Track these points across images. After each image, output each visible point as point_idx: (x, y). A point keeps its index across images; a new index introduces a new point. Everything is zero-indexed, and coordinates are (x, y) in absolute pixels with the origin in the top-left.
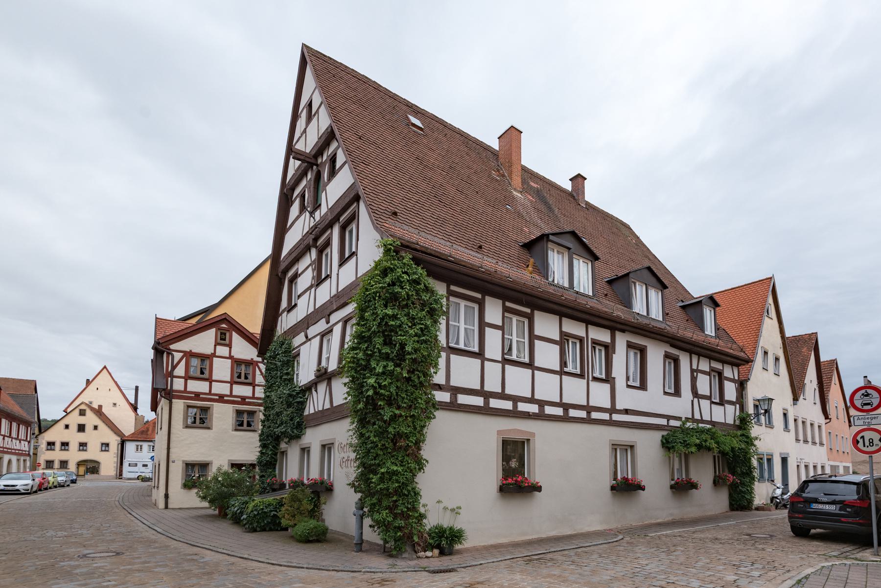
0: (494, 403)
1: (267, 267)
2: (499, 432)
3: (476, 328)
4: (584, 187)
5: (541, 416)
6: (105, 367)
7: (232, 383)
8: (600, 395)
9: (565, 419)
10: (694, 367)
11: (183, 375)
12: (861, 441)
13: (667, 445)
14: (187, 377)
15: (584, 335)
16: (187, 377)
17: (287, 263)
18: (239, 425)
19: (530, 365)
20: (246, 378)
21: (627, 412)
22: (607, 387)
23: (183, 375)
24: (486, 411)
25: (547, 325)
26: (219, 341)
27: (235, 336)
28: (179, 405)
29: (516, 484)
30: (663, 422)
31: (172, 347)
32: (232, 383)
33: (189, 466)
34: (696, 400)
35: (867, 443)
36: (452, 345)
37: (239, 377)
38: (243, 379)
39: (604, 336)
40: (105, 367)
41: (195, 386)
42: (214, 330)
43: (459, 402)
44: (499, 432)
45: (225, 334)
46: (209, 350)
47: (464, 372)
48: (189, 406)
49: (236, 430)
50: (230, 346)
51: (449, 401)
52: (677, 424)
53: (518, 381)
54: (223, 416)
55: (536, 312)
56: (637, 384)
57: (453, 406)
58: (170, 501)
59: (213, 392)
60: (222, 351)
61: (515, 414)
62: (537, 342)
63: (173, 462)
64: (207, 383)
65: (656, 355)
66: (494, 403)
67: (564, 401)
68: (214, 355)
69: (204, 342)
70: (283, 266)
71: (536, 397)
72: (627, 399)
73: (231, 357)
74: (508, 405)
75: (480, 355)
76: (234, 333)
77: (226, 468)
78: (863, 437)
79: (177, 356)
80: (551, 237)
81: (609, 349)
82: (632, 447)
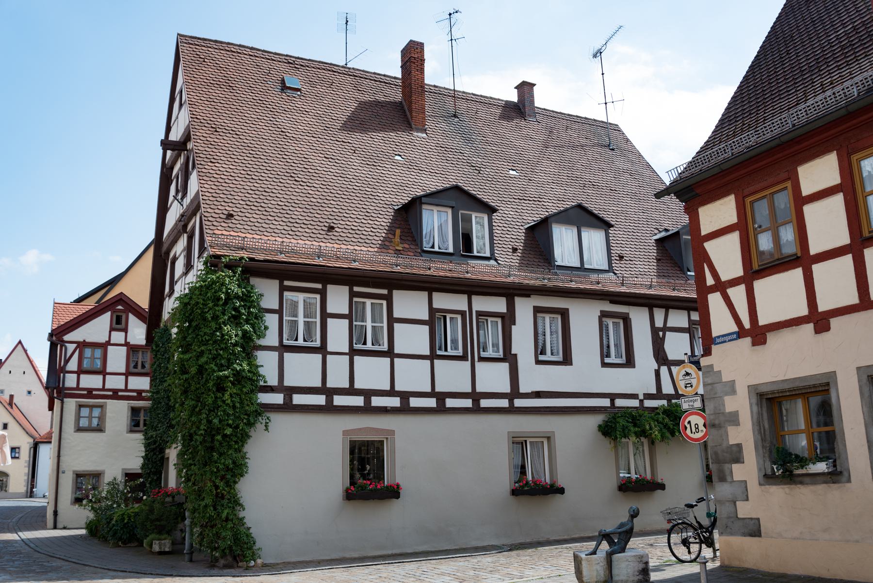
0: (339, 401)
1: (152, 249)
2: (345, 433)
4: (533, 96)
5: (405, 409)
6: (20, 342)
7: (128, 374)
8: (493, 378)
9: (441, 409)
10: (659, 323)
11: (76, 369)
12: (688, 426)
13: (607, 430)
14: (80, 371)
15: (465, 307)
16: (80, 371)
17: (169, 242)
18: (135, 426)
19: (390, 353)
20: (143, 367)
21: (538, 395)
22: (505, 367)
23: (76, 369)
24: (329, 409)
25: (410, 304)
26: (114, 325)
27: (131, 317)
28: (71, 404)
30: (606, 402)
31: (66, 338)
32: (128, 374)
33: (78, 475)
34: (664, 370)
35: (694, 430)
36: (285, 342)
37: (136, 367)
38: (139, 369)
39: (498, 305)
40: (20, 342)
41: (91, 381)
44: (345, 433)
46: (103, 339)
47: (302, 370)
48: (81, 406)
50: (125, 330)
52: (635, 403)
53: (372, 373)
54: (118, 413)
55: (395, 292)
56: (560, 358)
57: (288, 407)
58: (59, 518)
59: (107, 387)
61: (368, 409)
62: (396, 325)
63: (63, 472)
64: (101, 377)
65: (584, 320)
66: (339, 401)
67: (438, 389)
69: (97, 330)
71: (397, 388)
72: (533, 378)
73: (126, 344)
74: (359, 401)
75: (322, 350)
76: (130, 315)
77: (120, 478)
78: (689, 422)
79: (71, 347)
80: (424, 200)
81: (508, 319)
82: (548, 438)
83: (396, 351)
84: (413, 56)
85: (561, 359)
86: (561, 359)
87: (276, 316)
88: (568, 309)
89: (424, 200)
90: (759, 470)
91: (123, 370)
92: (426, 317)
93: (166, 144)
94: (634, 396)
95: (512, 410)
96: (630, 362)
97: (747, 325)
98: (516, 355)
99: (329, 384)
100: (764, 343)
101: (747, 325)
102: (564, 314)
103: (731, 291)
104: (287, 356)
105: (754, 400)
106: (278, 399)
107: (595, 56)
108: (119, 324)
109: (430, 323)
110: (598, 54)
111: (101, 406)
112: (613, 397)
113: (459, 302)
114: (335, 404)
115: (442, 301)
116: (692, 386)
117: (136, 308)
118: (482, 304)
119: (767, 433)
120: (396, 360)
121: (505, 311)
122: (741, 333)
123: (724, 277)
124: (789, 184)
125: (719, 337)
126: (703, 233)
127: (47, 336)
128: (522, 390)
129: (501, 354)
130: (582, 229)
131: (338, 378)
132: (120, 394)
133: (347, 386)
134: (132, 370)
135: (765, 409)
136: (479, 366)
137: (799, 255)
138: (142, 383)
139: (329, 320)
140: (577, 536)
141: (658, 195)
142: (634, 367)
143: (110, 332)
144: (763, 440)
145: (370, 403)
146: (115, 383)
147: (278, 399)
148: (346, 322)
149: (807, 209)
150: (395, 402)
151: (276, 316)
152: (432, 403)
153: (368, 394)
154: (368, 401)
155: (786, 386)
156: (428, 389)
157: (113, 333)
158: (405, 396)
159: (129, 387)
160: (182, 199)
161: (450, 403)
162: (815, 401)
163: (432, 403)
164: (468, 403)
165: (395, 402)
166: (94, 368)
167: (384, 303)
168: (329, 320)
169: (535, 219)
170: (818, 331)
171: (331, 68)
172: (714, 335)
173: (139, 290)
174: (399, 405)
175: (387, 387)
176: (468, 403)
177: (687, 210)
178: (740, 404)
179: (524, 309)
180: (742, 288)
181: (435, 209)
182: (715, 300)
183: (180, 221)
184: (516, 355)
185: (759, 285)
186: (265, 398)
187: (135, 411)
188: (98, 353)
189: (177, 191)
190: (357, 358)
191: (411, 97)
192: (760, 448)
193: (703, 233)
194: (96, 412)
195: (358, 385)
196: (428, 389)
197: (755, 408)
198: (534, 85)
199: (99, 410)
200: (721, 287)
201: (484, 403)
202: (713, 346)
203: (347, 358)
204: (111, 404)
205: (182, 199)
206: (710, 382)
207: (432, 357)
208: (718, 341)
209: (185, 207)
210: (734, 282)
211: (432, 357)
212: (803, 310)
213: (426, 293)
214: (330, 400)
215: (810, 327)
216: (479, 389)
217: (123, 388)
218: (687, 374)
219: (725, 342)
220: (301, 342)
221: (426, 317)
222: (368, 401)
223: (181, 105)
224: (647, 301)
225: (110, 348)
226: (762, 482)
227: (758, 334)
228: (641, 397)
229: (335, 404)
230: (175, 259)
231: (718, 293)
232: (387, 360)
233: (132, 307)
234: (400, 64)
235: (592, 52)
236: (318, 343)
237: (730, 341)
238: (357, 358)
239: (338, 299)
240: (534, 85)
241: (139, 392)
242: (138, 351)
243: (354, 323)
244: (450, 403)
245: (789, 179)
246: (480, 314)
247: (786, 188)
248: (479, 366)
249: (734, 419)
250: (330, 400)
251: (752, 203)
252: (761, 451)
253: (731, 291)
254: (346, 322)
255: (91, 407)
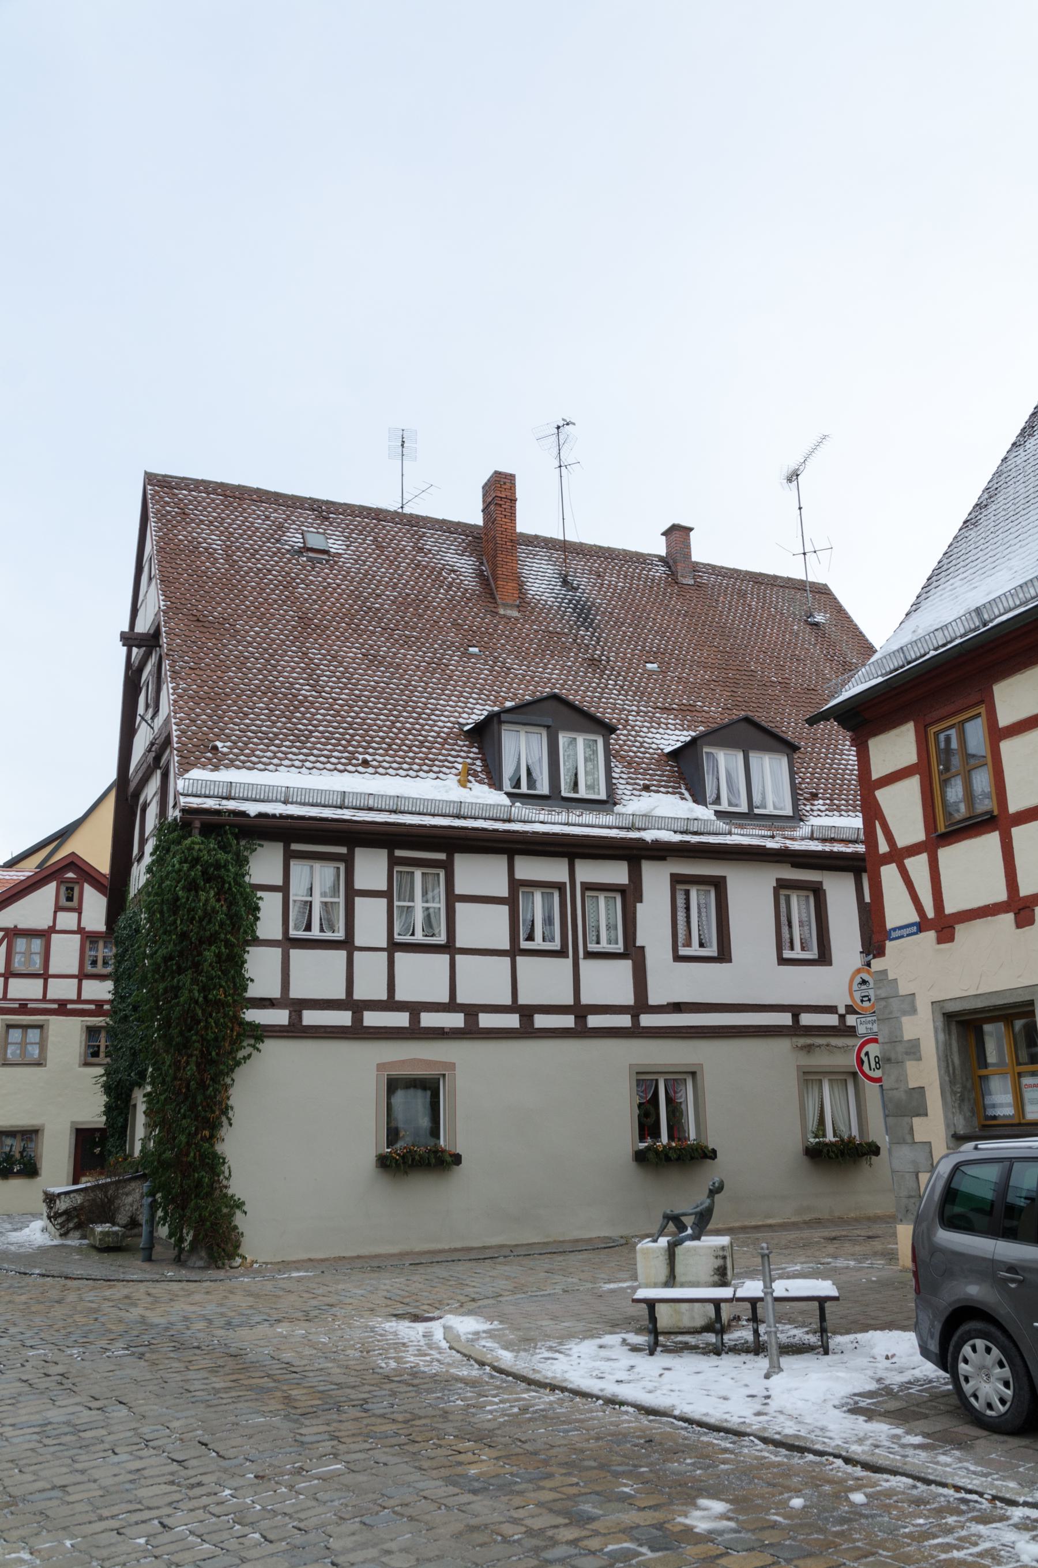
2: (380, 1067)
3: (341, 900)
5: (471, 1032)
7: (82, 976)
9: (527, 1031)
19: (449, 948)
21: (677, 1008)
24: (357, 1032)
26: (63, 902)
29: (415, 1155)
32: (82, 976)
36: (293, 933)
38: (100, 969)
39: (617, 873)
42: (54, 884)
43: (305, 1022)
44: (380, 1067)
45: (72, 889)
46: (44, 923)
47: (317, 975)
48: (9, 1026)
49: (86, 1064)
50: (79, 910)
51: (286, 1023)
53: (422, 978)
54: (67, 1035)
57: (295, 1031)
59: (49, 997)
60: (67, 920)
61: (415, 1033)
65: (751, 895)
66: (372, 1019)
67: (522, 1000)
68: (52, 930)
70: (133, 785)
71: (460, 999)
72: (668, 981)
73: (80, 930)
75: (347, 944)
76: (86, 886)
78: (867, 1054)
80: (503, 717)
81: (630, 895)
82: (693, 1074)
83: (458, 945)
84: (500, 492)
85: (715, 954)
86: (715, 954)
87: (279, 896)
88: (724, 878)
89: (503, 717)
90: (947, 1126)
91: (75, 971)
92: (504, 893)
93: (129, 639)
94: (831, 1009)
95: (636, 1032)
96: (824, 958)
97: (930, 914)
98: (643, 948)
99: (357, 996)
100: (951, 939)
101: (930, 914)
102: (719, 885)
103: (909, 862)
104: (294, 953)
105: (940, 1024)
106: (280, 1017)
107: (790, 480)
108: (69, 901)
109: (511, 902)
110: (793, 476)
111: (40, 1027)
112: (796, 1011)
113: (555, 871)
114: (366, 1024)
115: (528, 869)
116: (869, 1000)
117: (93, 874)
118: (589, 872)
119: (958, 1072)
120: (458, 957)
121: (626, 882)
122: (922, 925)
123: (901, 842)
124: (982, 709)
125: (894, 929)
126: (875, 776)
127: (676, 522)
128: (653, 1000)
129: (619, 947)
130: (751, 755)
131: (370, 985)
132: (69, 1006)
133: (385, 997)
134: (89, 969)
135: (954, 1037)
136: (585, 965)
137: (996, 813)
138: (101, 990)
139: (358, 901)
140: (737, 1224)
141: (812, 721)
142: (830, 964)
143: (55, 912)
144: (952, 1083)
145: (419, 1022)
146: (62, 990)
147: (280, 1017)
148: (384, 902)
149: (1006, 747)
150: (456, 1020)
151: (279, 896)
152: (512, 1021)
153: (415, 1009)
154: (415, 1019)
155: (979, 1004)
156: (507, 1001)
157: (60, 914)
158: (472, 1011)
159: (84, 997)
160: (153, 718)
161: (541, 1021)
162: (1019, 1024)
163: (512, 1021)
164: (568, 1021)
165: (456, 1020)
166: (32, 970)
167: (442, 874)
168: (358, 901)
169: (683, 739)
170: (1020, 924)
171: (378, 515)
172: (889, 925)
173: (96, 849)
174: (462, 1025)
175: (445, 999)
176: (568, 1021)
177: (854, 742)
178: (922, 1028)
179: (656, 879)
180: (923, 858)
181: (523, 729)
182: (889, 873)
183: (150, 751)
184: (643, 948)
185: (945, 854)
186: (253, 1016)
187: (92, 1032)
188: (37, 944)
189: (147, 706)
190: (398, 956)
191: (495, 557)
192: (948, 1095)
193: (875, 776)
194: (33, 1035)
195: (400, 996)
196: (507, 1001)
197: (941, 1037)
198: (691, 529)
199: (37, 1031)
200: (898, 856)
201: (594, 1021)
202: (887, 942)
203: (384, 955)
204: (57, 1024)
205: (153, 718)
206: (883, 995)
207: (514, 952)
208: (894, 935)
209: (156, 731)
210: (913, 850)
211: (514, 952)
212: (1001, 895)
213: (505, 857)
214: (357, 1019)
215: (1009, 918)
216: (585, 1000)
217: (75, 997)
218: (864, 982)
219: (902, 937)
220: (315, 933)
221: (504, 893)
222: (415, 1019)
223: (150, 579)
224: (851, 863)
225: (54, 936)
226: (951, 1145)
227: (944, 926)
228: (842, 1010)
229: (366, 1024)
230: (145, 806)
231: (894, 865)
232: (445, 958)
233: (85, 873)
234: (481, 507)
235: (786, 472)
236: (340, 935)
237: (908, 935)
238: (398, 956)
239: (371, 869)
240: (691, 529)
241: (99, 1004)
242: (97, 942)
243: (396, 903)
244: (541, 1021)
245: (982, 702)
246: (587, 887)
247: (979, 715)
248: (585, 965)
249: (914, 1050)
250: (357, 1019)
251: (937, 734)
252: (949, 1099)
253: (909, 862)
254: (384, 902)
255: (25, 1027)
